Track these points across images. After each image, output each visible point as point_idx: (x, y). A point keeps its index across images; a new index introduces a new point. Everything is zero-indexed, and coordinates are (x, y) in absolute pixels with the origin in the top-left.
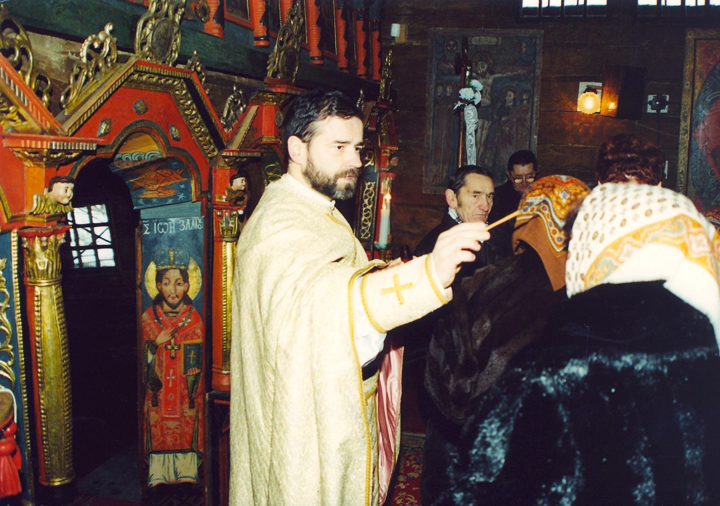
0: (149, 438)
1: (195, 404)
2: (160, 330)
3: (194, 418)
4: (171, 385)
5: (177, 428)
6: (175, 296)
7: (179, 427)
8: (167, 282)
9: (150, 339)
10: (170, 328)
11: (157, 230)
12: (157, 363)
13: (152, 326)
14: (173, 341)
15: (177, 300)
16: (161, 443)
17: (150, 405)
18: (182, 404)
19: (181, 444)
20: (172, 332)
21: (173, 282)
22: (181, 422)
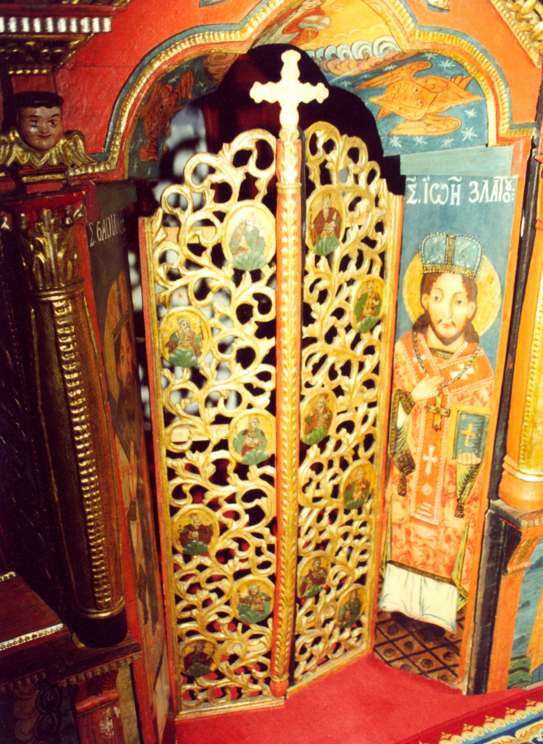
0: (389, 540)
1: (465, 512)
2: (421, 377)
4: (428, 470)
5: (431, 540)
7: (434, 539)
8: (439, 296)
10: (436, 378)
11: (429, 198)
14: (439, 400)
16: (405, 554)
19: (434, 566)
20: (440, 385)
21: (448, 297)
22: (439, 533)
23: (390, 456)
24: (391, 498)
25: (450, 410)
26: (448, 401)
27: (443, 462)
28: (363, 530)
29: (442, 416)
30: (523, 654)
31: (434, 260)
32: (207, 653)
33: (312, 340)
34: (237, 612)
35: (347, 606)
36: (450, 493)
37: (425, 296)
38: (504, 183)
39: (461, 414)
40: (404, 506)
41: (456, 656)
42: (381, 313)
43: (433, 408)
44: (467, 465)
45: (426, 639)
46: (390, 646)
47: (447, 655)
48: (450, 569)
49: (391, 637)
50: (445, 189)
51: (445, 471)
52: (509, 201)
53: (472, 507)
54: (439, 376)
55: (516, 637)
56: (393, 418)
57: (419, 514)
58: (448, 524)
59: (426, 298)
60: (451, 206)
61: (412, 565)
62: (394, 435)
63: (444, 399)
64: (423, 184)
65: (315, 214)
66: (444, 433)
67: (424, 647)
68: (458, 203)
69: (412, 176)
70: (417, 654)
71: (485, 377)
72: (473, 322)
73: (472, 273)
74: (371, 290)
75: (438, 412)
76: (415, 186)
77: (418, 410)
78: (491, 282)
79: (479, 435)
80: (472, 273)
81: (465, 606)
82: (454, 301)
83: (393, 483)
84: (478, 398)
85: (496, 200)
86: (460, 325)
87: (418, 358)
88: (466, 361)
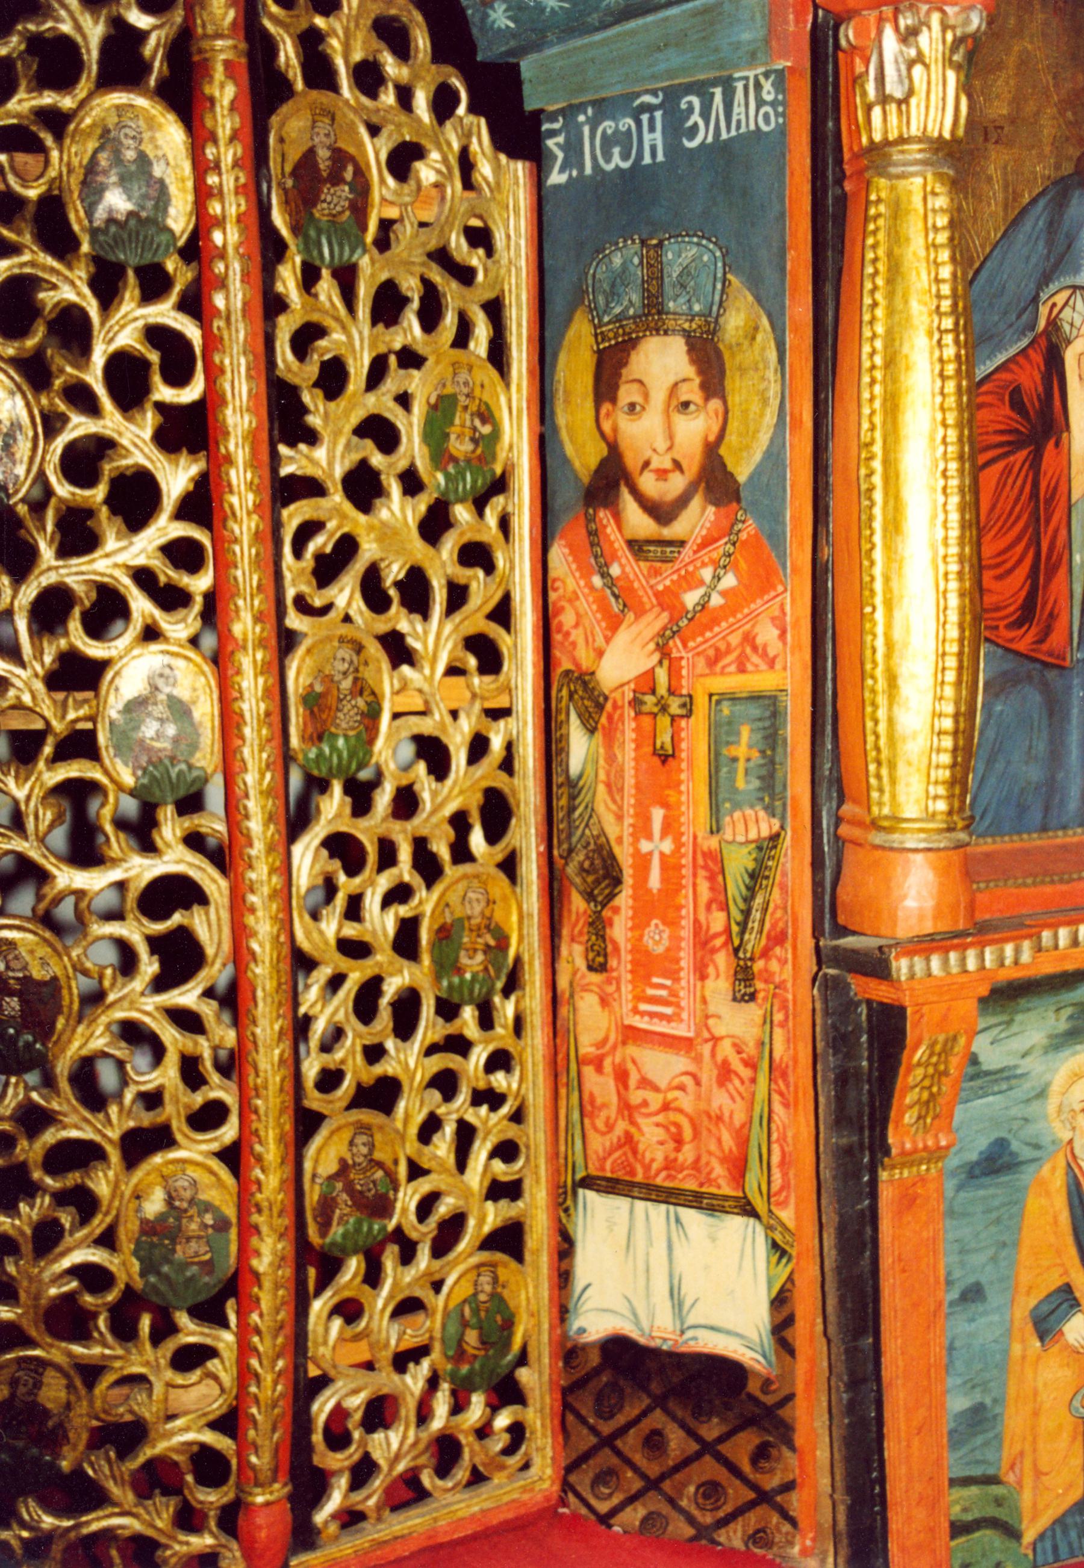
0: (576, 1115)
1: (759, 985)
2: (614, 624)
3: (751, 1049)
4: (655, 880)
5: (682, 1088)
6: (668, 464)
7: (688, 1081)
8: (638, 398)
9: (577, 665)
10: (649, 617)
11: (594, 158)
12: (602, 776)
13: (583, 604)
14: (662, 676)
15: (677, 484)
16: (620, 1146)
17: (581, 964)
18: (703, 976)
19: (696, 1164)
20: (661, 634)
21: (658, 397)
22: (698, 1059)
23: (559, 862)
24: (571, 984)
25: (690, 696)
26: (684, 672)
27: (688, 850)
28: (499, 1080)
29: (673, 718)
30: (991, 1471)
31: (618, 310)
32: (50, 1405)
33: (312, 488)
34: (136, 1266)
35: (467, 1311)
36: (716, 936)
37: (606, 407)
38: (758, 86)
39: (718, 702)
40: (604, 1002)
41: (787, 1453)
42: (502, 455)
43: (650, 699)
44: (748, 842)
45: (700, 1412)
46: (606, 1458)
47: (761, 1454)
48: (739, 1168)
49: (606, 1428)
50: (629, 129)
51: (695, 875)
52: (773, 125)
53: (774, 965)
54: (657, 609)
55: (958, 1403)
56: (560, 751)
57: (643, 1014)
58: (720, 1030)
59: (608, 415)
60: (648, 166)
61: (639, 1177)
62: (563, 802)
63: (674, 672)
64: (579, 127)
65: (294, 155)
66: (684, 765)
67: (698, 1439)
68: (660, 158)
69: (552, 117)
70: (677, 1468)
71: (763, 591)
72: (723, 451)
73: (708, 323)
74: (465, 390)
75: (664, 709)
76: (561, 139)
77: (616, 717)
78: (754, 338)
79: (769, 753)
80: (708, 323)
81: (790, 1279)
82: (674, 403)
83: (573, 939)
84: (755, 649)
85: (743, 130)
86: (693, 467)
87: (603, 576)
88: (715, 555)
